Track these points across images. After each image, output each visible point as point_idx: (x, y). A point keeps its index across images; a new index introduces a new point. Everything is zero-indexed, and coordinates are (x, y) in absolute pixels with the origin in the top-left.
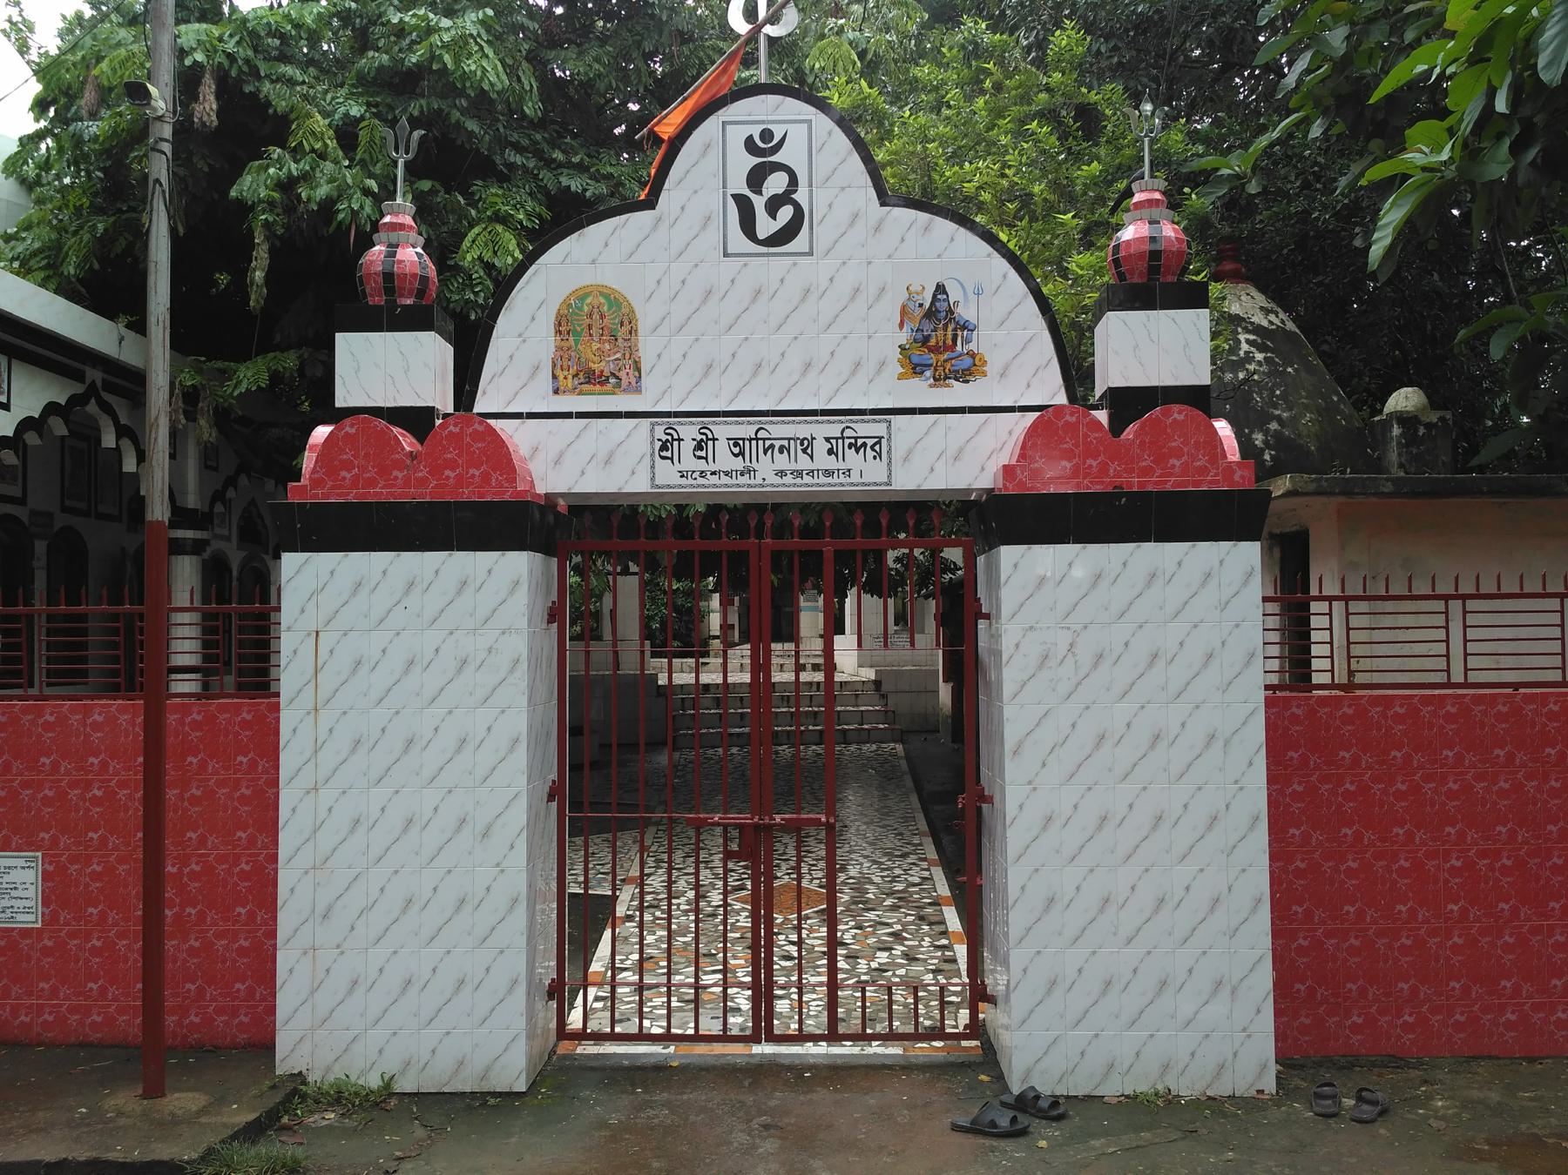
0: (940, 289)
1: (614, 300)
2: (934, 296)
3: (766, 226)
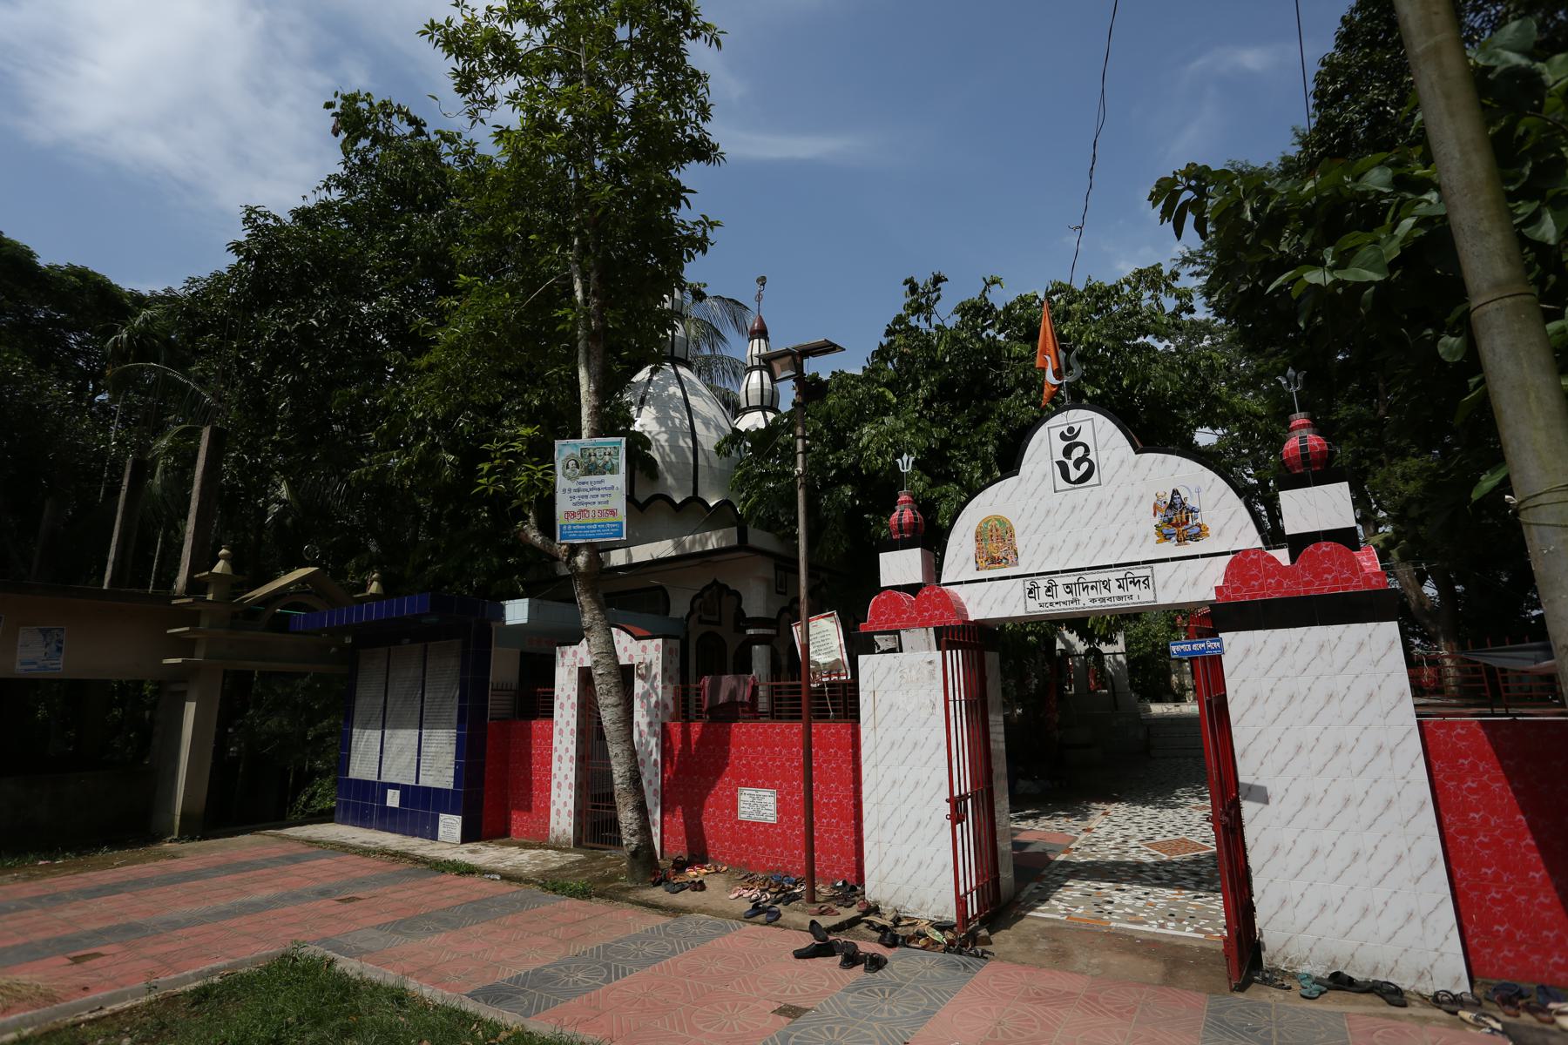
0: (1175, 492)
1: (1002, 521)
3: (1074, 474)
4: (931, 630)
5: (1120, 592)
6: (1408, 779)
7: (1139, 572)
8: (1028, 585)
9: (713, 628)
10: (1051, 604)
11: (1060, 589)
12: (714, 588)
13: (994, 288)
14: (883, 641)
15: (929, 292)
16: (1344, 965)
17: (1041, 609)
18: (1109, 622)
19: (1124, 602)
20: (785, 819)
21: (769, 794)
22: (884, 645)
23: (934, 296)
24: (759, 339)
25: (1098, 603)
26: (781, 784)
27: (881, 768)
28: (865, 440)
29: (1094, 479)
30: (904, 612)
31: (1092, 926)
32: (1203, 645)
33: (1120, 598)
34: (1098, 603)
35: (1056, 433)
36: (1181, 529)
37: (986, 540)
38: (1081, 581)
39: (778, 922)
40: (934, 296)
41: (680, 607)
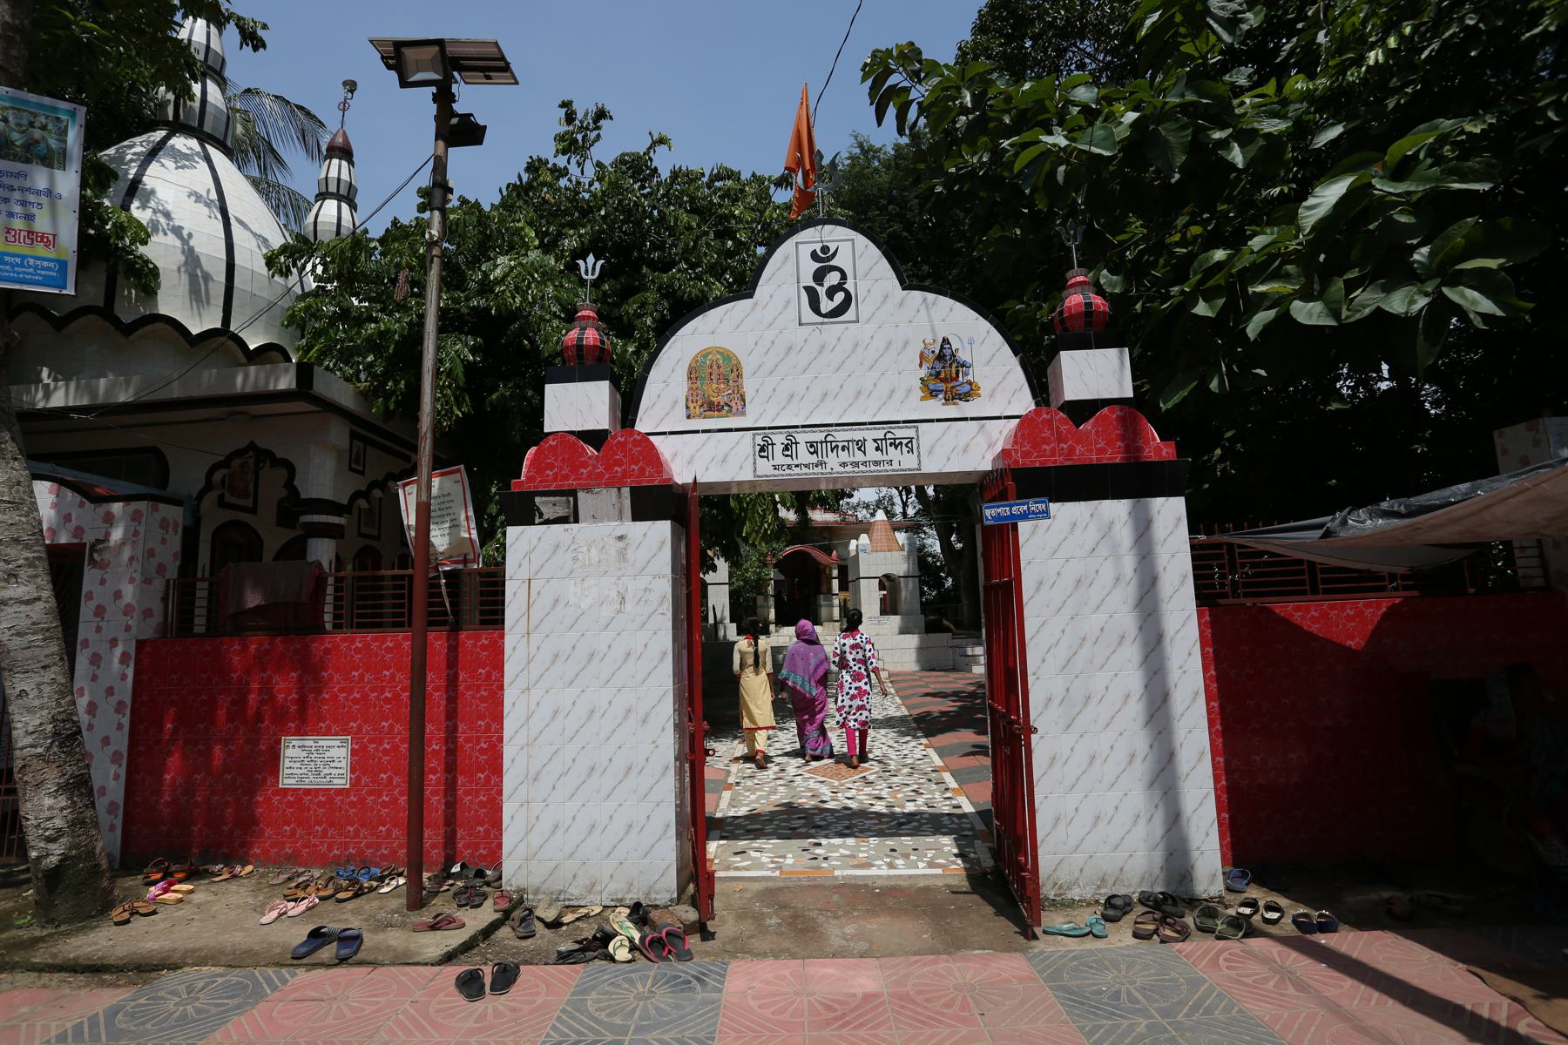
0: (945, 341)
1: (727, 355)
2: (942, 346)
3: (826, 305)
4: (626, 491)
5: (878, 456)
6: (1184, 669)
7: (900, 433)
8: (759, 440)
9: (242, 516)
10: (789, 467)
11: (802, 448)
12: (251, 453)
13: (661, 149)
14: (547, 507)
15: (587, 129)
16: (1045, 877)
17: (776, 472)
18: (766, 530)
19: (882, 468)
20: (364, 779)
21: (338, 743)
22: (548, 512)
23: (593, 135)
24: (340, 159)
25: (849, 468)
26: (360, 729)
27: (536, 693)
28: (498, 272)
29: (850, 314)
30: (585, 465)
31: (815, 879)
32: (1025, 508)
33: (877, 463)
34: (849, 468)
35: (806, 251)
36: (950, 385)
37: (703, 379)
38: (829, 438)
39: (360, 956)
40: (593, 135)
41: (188, 474)
